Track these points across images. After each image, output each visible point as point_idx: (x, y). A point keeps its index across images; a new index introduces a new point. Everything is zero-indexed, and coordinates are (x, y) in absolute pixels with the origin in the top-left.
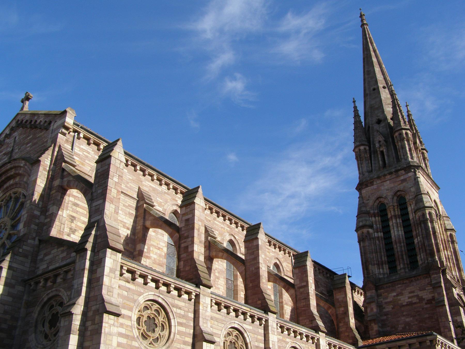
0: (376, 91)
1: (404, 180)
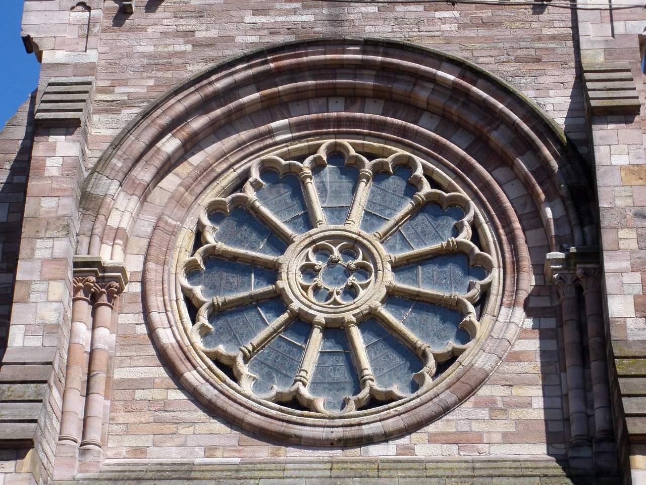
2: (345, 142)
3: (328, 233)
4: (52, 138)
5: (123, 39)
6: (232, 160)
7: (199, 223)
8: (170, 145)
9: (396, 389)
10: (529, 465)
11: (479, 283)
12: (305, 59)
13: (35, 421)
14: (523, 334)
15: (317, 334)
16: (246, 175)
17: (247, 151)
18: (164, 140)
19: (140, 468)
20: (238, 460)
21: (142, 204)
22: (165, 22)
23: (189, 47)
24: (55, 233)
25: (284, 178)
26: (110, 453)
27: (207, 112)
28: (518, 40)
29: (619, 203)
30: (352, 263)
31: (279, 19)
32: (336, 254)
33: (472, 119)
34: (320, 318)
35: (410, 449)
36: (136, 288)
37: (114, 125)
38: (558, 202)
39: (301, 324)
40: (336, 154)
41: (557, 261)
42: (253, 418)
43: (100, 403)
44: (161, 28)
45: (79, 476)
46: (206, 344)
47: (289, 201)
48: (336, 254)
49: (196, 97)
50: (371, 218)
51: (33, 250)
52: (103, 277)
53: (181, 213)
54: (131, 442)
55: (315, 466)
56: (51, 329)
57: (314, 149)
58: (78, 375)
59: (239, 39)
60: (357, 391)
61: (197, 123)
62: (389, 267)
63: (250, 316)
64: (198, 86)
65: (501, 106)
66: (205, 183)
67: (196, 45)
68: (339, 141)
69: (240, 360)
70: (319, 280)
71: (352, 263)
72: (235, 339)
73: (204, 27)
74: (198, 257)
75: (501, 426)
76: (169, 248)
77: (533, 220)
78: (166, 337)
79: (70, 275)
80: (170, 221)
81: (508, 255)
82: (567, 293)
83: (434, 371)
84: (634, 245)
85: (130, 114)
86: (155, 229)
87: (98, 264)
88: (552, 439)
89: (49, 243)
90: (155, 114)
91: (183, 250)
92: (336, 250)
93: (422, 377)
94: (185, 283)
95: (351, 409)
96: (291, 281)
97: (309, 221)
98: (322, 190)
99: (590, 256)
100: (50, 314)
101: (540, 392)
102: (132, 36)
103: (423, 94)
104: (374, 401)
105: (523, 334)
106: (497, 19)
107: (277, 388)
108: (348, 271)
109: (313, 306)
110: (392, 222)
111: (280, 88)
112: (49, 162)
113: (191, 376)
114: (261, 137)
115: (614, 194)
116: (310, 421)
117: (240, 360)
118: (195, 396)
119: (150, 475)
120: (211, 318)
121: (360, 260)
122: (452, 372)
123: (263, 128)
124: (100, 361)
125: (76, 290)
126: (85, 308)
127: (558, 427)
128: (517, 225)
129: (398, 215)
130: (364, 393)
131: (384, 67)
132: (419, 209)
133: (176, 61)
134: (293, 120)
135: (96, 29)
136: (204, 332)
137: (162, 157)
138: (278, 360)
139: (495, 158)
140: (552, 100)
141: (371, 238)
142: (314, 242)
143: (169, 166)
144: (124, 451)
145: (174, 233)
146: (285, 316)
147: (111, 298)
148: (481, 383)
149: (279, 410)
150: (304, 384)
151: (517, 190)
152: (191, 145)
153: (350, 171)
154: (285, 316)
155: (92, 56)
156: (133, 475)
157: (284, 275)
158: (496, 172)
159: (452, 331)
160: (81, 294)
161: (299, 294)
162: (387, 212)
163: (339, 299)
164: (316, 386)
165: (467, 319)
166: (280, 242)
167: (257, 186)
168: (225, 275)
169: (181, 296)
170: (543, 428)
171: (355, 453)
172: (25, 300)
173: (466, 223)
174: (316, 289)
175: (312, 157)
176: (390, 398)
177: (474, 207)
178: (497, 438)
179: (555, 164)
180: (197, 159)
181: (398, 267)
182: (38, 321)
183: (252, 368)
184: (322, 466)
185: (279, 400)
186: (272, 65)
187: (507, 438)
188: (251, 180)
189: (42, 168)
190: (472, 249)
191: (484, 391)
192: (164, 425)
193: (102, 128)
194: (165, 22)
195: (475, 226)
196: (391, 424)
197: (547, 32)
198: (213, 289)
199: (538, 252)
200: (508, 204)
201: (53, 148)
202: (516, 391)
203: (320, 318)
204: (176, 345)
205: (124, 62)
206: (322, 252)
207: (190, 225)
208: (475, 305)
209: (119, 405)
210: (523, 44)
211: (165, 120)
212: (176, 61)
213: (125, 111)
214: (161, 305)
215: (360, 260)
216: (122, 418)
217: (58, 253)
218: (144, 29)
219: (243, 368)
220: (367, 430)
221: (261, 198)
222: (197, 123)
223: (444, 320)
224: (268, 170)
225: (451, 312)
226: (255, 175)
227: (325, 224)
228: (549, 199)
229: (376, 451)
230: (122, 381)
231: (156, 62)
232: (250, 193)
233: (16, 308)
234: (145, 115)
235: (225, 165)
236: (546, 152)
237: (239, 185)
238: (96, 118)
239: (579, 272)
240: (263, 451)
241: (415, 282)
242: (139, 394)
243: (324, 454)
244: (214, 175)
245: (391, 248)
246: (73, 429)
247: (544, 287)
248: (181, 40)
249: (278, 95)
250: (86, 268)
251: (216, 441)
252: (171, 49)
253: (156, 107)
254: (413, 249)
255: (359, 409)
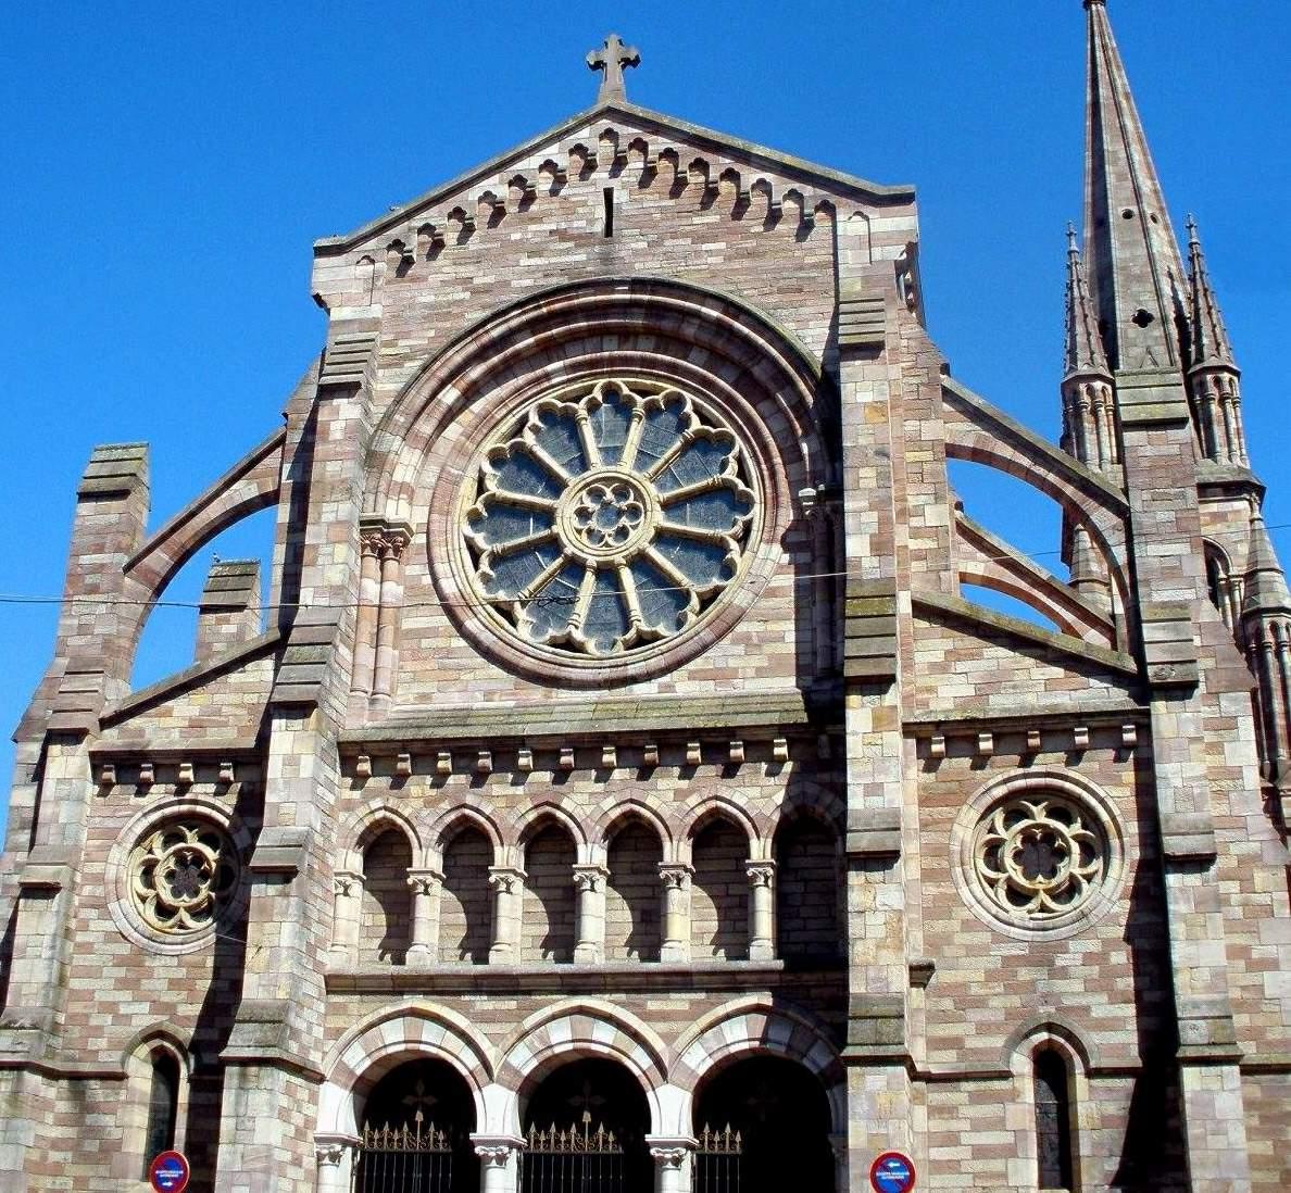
0: (1136, 220)
1: (1218, 517)
2: (618, 380)
3: (600, 476)
4: (336, 402)
5: (406, 290)
6: (511, 406)
7: (480, 470)
8: (450, 395)
9: (661, 629)
10: (776, 699)
11: (741, 519)
12: (576, 301)
13: (318, 683)
14: (780, 569)
15: (589, 578)
16: (524, 420)
17: (525, 396)
18: (444, 391)
19: (424, 715)
20: (512, 704)
21: (426, 455)
22: (445, 270)
23: (467, 295)
24: (339, 496)
25: (560, 421)
26: (399, 700)
27: (485, 360)
28: (780, 270)
29: (862, 441)
30: (623, 505)
31: (553, 260)
32: (609, 496)
33: (736, 355)
34: (592, 561)
35: (670, 687)
36: (420, 539)
37: (397, 379)
38: (813, 436)
39: (575, 568)
40: (611, 393)
41: (809, 498)
42: (527, 663)
43: (388, 653)
44: (441, 277)
45: (369, 724)
46: (489, 590)
47: (566, 442)
48: (609, 496)
49: (472, 348)
50: (644, 458)
51: (320, 514)
52: (389, 533)
53: (462, 462)
54: (418, 689)
55: (580, 708)
56: (337, 590)
57: (590, 390)
58: (367, 628)
59: (514, 283)
60: (627, 629)
61: (476, 372)
62: (658, 507)
63: (527, 561)
64: (474, 335)
65: (761, 341)
66: (485, 431)
67: (475, 292)
68: (613, 380)
69: (517, 606)
70: (593, 523)
71: (623, 505)
72: (515, 584)
73: (481, 273)
74: (480, 506)
75: (758, 661)
76: (452, 498)
77: (792, 455)
78: (448, 586)
79: (356, 535)
80: (453, 471)
81: (769, 491)
82: (819, 527)
83: (698, 608)
84: (873, 484)
85: (413, 366)
86: (439, 478)
87: (382, 522)
88: (801, 671)
89: (334, 506)
90: (435, 367)
91: (467, 499)
92: (608, 491)
93: (685, 615)
94: (468, 530)
95: (620, 650)
96: (566, 526)
97: (583, 463)
98: (598, 431)
99: (834, 493)
100: (335, 576)
101: (793, 627)
102: (414, 286)
103: (690, 331)
104: (642, 640)
105: (780, 569)
106: (761, 249)
107: (552, 632)
108: (620, 513)
109: (586, 550)
110: (661, 461)
111: (554, 331)
112: (333, 426)
113: (471, 624)
114: (538, 380)
115: (857, 434)
116: (580, 663)
117: (517, 606)
118: (476, 644)
119: (431, 722)
120: (493, 565)
121: (631, 500)
122: (712, 610)
123: (539, 372)
124: (388, 614)
125: (364, 547)
126: (373, 564)
127: (807, 660)
128: (778, 460)
129: (667, 456)
130: (632, 634)
131: (651, 304)
132: (688, 446)
133: (455, 310)
134: (568, 361)
135: (379, 284)
136: (486, 579)
137: (443, 409)
138: (554, 604)
139: (758, 393)
140: (810, 332)
141: (642, 480)
142: (588, 485)
143: (450, 415)
144: (411, 697)
145: (456, 483)
146: (560, 560)
147: (397, 551)
148: (738, 619)
149: (553, 653)
150: (577, 627)
151: (779, 426)
152: (472, 393)
153: (623, 408)
154: (560, 560)
155: (376, 311)
156: (415, 723)
157: (558, 520)
158: (762, 406)
159: (715, 566)
160: (368, 551)
161: (572, 538)
162: (659, 450)
163: (610, 541)
164: (589, 627)
165: (728, 556)
166: (556, 486)
167: (535, 430)
168: (505, 521)
169: (464, 545)
170: (794, 662)
171: (621, 693)
172: (313, 564)
173: (731, 460)
174: (590, 532)
175: (585, 399)
176: (655, 637)
177: (739, 442)
178: (751, 672)
179: (810, 400)
180: (478, 406)
181: (668, 506)
182: (326, 583)
183: (530, 613)
184: (587, 708)
185: (554, 643)
186: (544, 310)
187: (760, 673)
188: (529, 424)
189: (326, 432)
190: (736, 486)
191: (741, 628)
192: (448, 674)
193: (386, 384)
194: (445, 270)
195: (740, 460)
196: (655, 664)
197: (809, 260)
198: (494, 536)
199: (795, 486)
200: (770, 440)
201: (337, 411)
202: (772, 626)
203: (592, 561)
204: (458, 594)
205: (408, 313)
206: (596, 495)
207: (473, 474)
208: (739, 541)
209: (407, 654)
210: (785, 274)
211: (443, 373)
212: (455, 310)
213: (407, 365)
214: (444, 554)
215: (631, 500)
216: (410, 666)
217: (342, 516)
218: (425, 279)
219: (521, 613)
220: (631, 670)
221: (539, 440)
222: (476, 372)
223: (709, 558)
224: (546, 413)
225: (716, 549)
226: (534, 419)
227: (598, 466)
228: (806, 434)
229: (641, 690)
230: (410, 631)
231: (436, 313)
232: (529, 438)
233: (305, 571)
234: (425, 369)
235: (504, 411)
236: (802, 386)
237: (518, 430)
238: (380, 373)
239: (828, 509)
240: (537, 694)
241: (683, 520)
242: (425, 643)
243: (592, 695)
244: (494, 421)
245: (662, 487)
246: (364, 682)
247: (800, 523)
248: (460, 288)
249: (551, 338)
250: (369, 525)
251: (493, 686)
252: (450, 297)
253: (435, 359)
254: (680, 486)
255: (627, 649)
